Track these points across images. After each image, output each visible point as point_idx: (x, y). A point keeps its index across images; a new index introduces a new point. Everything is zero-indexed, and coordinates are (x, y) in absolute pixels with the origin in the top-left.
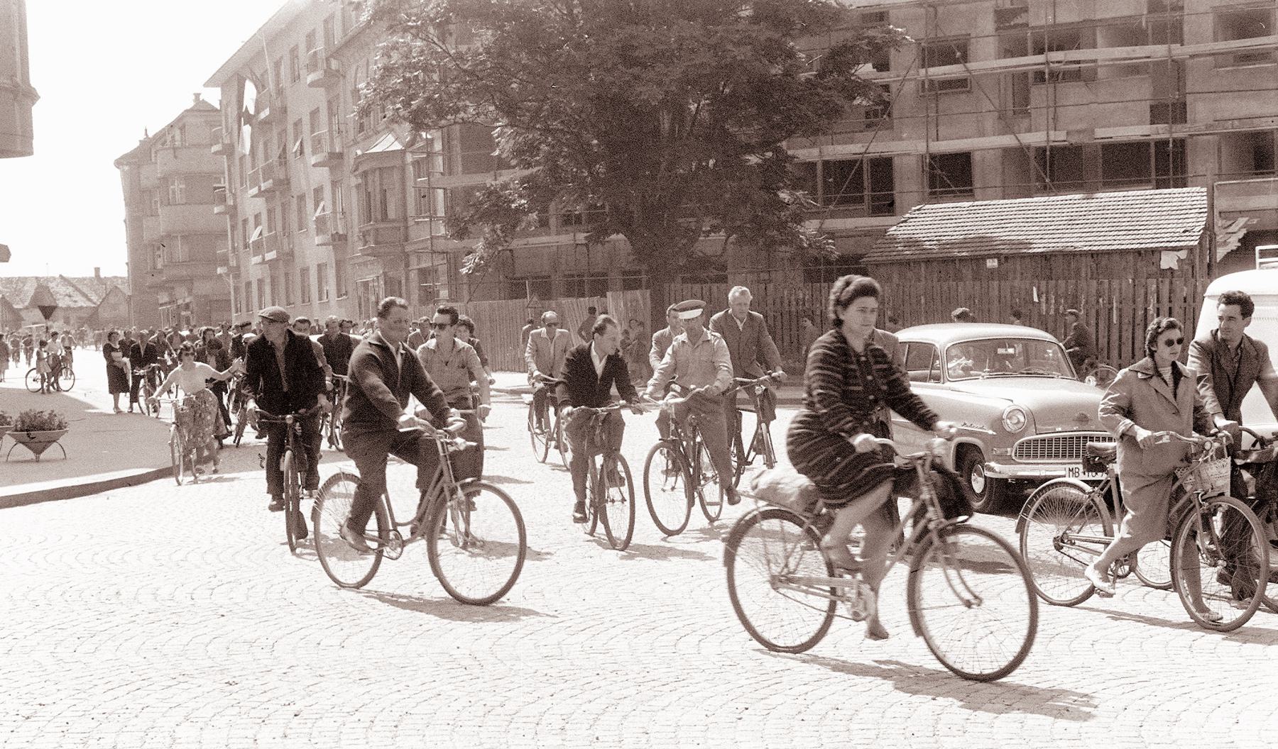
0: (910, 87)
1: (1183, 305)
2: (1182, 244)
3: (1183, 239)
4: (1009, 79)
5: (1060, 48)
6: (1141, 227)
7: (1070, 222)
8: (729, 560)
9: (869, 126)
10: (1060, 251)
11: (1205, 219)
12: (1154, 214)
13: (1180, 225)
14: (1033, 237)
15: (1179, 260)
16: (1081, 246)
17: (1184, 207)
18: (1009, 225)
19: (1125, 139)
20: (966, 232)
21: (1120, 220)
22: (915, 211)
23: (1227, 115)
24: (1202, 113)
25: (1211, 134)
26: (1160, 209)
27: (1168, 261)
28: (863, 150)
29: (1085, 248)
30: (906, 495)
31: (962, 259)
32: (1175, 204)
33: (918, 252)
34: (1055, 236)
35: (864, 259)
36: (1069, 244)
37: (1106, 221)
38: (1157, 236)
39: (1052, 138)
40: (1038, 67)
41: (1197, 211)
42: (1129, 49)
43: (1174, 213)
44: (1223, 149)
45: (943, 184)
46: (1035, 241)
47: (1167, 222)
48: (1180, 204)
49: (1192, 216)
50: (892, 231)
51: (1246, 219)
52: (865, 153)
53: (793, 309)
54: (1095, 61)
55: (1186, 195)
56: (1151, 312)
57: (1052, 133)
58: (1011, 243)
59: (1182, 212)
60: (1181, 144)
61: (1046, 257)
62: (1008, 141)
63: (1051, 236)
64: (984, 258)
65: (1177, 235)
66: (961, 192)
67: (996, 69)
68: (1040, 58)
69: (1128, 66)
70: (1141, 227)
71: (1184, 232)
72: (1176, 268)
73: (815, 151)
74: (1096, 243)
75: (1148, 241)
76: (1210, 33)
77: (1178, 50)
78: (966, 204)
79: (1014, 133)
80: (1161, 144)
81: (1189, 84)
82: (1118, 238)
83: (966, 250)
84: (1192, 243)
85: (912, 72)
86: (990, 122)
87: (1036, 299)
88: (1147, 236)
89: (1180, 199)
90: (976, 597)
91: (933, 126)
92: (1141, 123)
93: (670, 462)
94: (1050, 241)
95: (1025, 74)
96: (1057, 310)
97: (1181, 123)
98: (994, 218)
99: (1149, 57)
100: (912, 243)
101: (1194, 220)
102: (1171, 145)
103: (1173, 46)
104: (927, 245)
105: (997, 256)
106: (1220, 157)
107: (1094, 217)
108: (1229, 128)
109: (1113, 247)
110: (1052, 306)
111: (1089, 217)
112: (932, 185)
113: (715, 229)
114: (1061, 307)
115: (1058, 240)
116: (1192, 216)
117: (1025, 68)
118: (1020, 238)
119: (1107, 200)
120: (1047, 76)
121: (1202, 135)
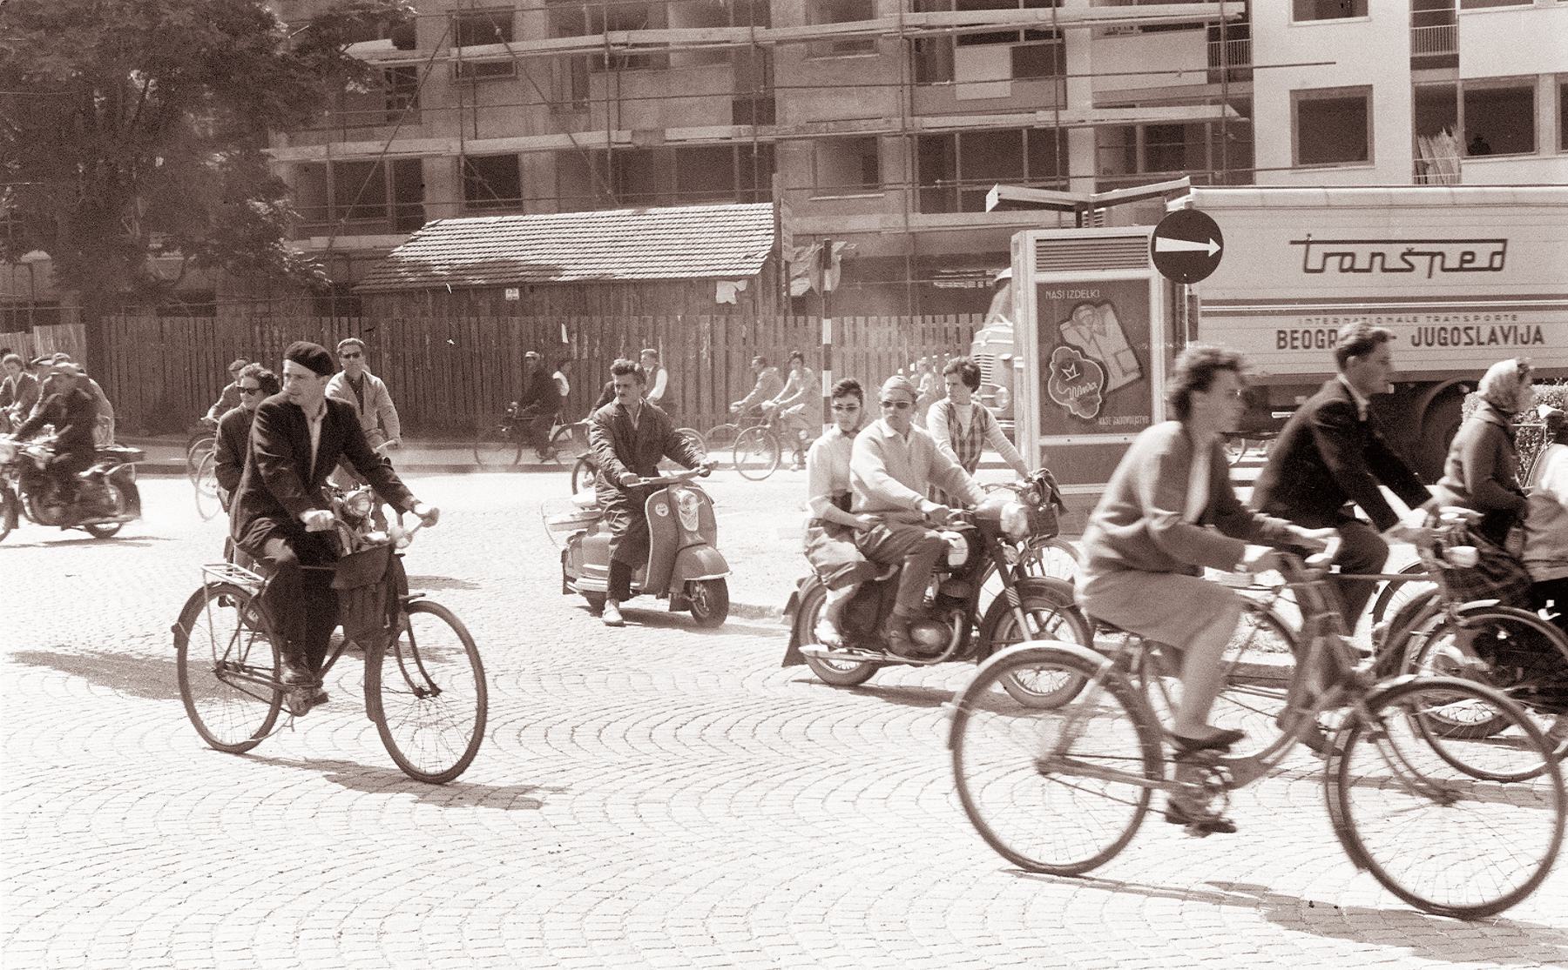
0: (440, 71)
1: (743, 348)
2: (741, 272)
3: (742, 266)
4: (568, 62)
5: (624, 27)
6: (696, 252)
7: (614, 244)
8: (955, 741)
9: (391, 119)
10: (597, 280)
11: (771, 242)
12: (714, 235)
13: (742, 250)
14: (567, 261)
15: (737, 293)
16: (621, 273)
17: (750, 228)
18: (540, 247)
19: (701, 142)
20: (487, 255)
21: (673, 242)
22: (429, 227)
23: (822, 116)
24: (793, 111)
25: (803, 139)
26: (721, 229)
27: (725, 294)
28: (382, 149)
29: (627, 277)
30: (283, 565)
31: (478, 289)
32: (740, 223)
33: (424, 279)
34: (594, 261)
35: (357, 288)
36: (608, 271)
37: (657, 242)
38: (713, 262)
39: (614, 139)
40: (597, 49)
41: (763, 232)
42: (704, 30)
43: (737, 234)
44: (819, 156)
45: (485, 194)
46: (568, 267)
47: (727, 245)
48: (746, 223)
49: (757, 238)
50: (397, 252)
51: (843, 243)
52: (385, 153)
53: (267, 350)
54: (667, 44)
55: (755, 212)
56: (704, 357)
57: (614, 132)
58: (539, 268)
59: (747, 233)
60: (768, 150)
61: (580, 286)
62: (560, 141)
63: (588, 261)
64: (501, 288)
65: (737, 261)
66: (509, 204)
67: (545, 51)
68: (598, 39)
69: (704, 52)
70: (696, 252)
71: (746, 257)
72: (734, 302)
73: (322, 150)
74: (641, 270)
75: (702, 268)
76: (801, 15)
77: (761, 32)
78: (493, 219)
79: (569, 133)
80: (746, 149)
81: (777, 77)
82: (668, 264)
83: (483, 276)
84: (752, 272)
85: (442, 51)
86: (540, 117)
87: (565, 340)
88: (701, 263)
89: (747, 217)
90: (432, 685)
91: (469, 119)
92: (722, 123)
93: (1029, 574)
94: (586, 266)
95: (583, 58)
96: (591, 353)
97: (769, 123)
98: (523, 238)
99: (728, 42)
100: (420, 267)
101: (759, 243)
102: (755, 152)
103: (757, 29)
104: (436, 270)
105: (521, 286)
106: (815, 166)
107: (643, 238)
108: (834, 131)
109: (660, 276)
110: (586, 348)
111: (638, 238)
112: (470, 194)
113: (167, 247)
114: (596, 350)
115: (596, 266)
116: (757, 238)
117: (581, 51)
118: (551, 262)
119: (662, 217)
120: (606, 62)
121: (794, 139)
